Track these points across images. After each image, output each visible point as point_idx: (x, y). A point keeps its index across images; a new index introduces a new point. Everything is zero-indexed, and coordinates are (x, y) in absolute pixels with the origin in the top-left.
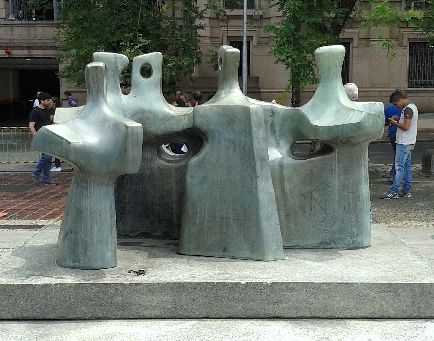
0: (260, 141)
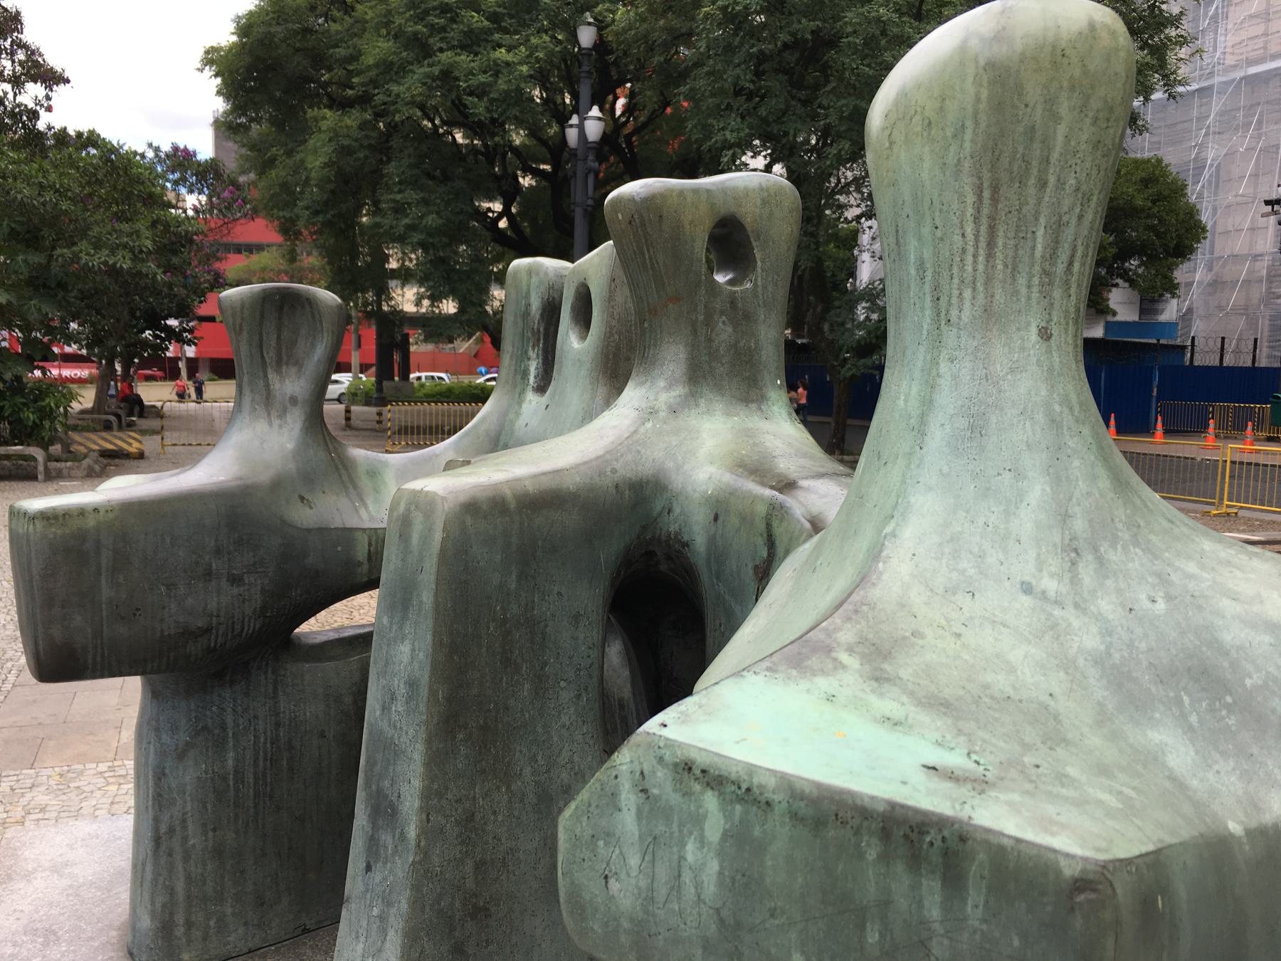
0: (393, 698)
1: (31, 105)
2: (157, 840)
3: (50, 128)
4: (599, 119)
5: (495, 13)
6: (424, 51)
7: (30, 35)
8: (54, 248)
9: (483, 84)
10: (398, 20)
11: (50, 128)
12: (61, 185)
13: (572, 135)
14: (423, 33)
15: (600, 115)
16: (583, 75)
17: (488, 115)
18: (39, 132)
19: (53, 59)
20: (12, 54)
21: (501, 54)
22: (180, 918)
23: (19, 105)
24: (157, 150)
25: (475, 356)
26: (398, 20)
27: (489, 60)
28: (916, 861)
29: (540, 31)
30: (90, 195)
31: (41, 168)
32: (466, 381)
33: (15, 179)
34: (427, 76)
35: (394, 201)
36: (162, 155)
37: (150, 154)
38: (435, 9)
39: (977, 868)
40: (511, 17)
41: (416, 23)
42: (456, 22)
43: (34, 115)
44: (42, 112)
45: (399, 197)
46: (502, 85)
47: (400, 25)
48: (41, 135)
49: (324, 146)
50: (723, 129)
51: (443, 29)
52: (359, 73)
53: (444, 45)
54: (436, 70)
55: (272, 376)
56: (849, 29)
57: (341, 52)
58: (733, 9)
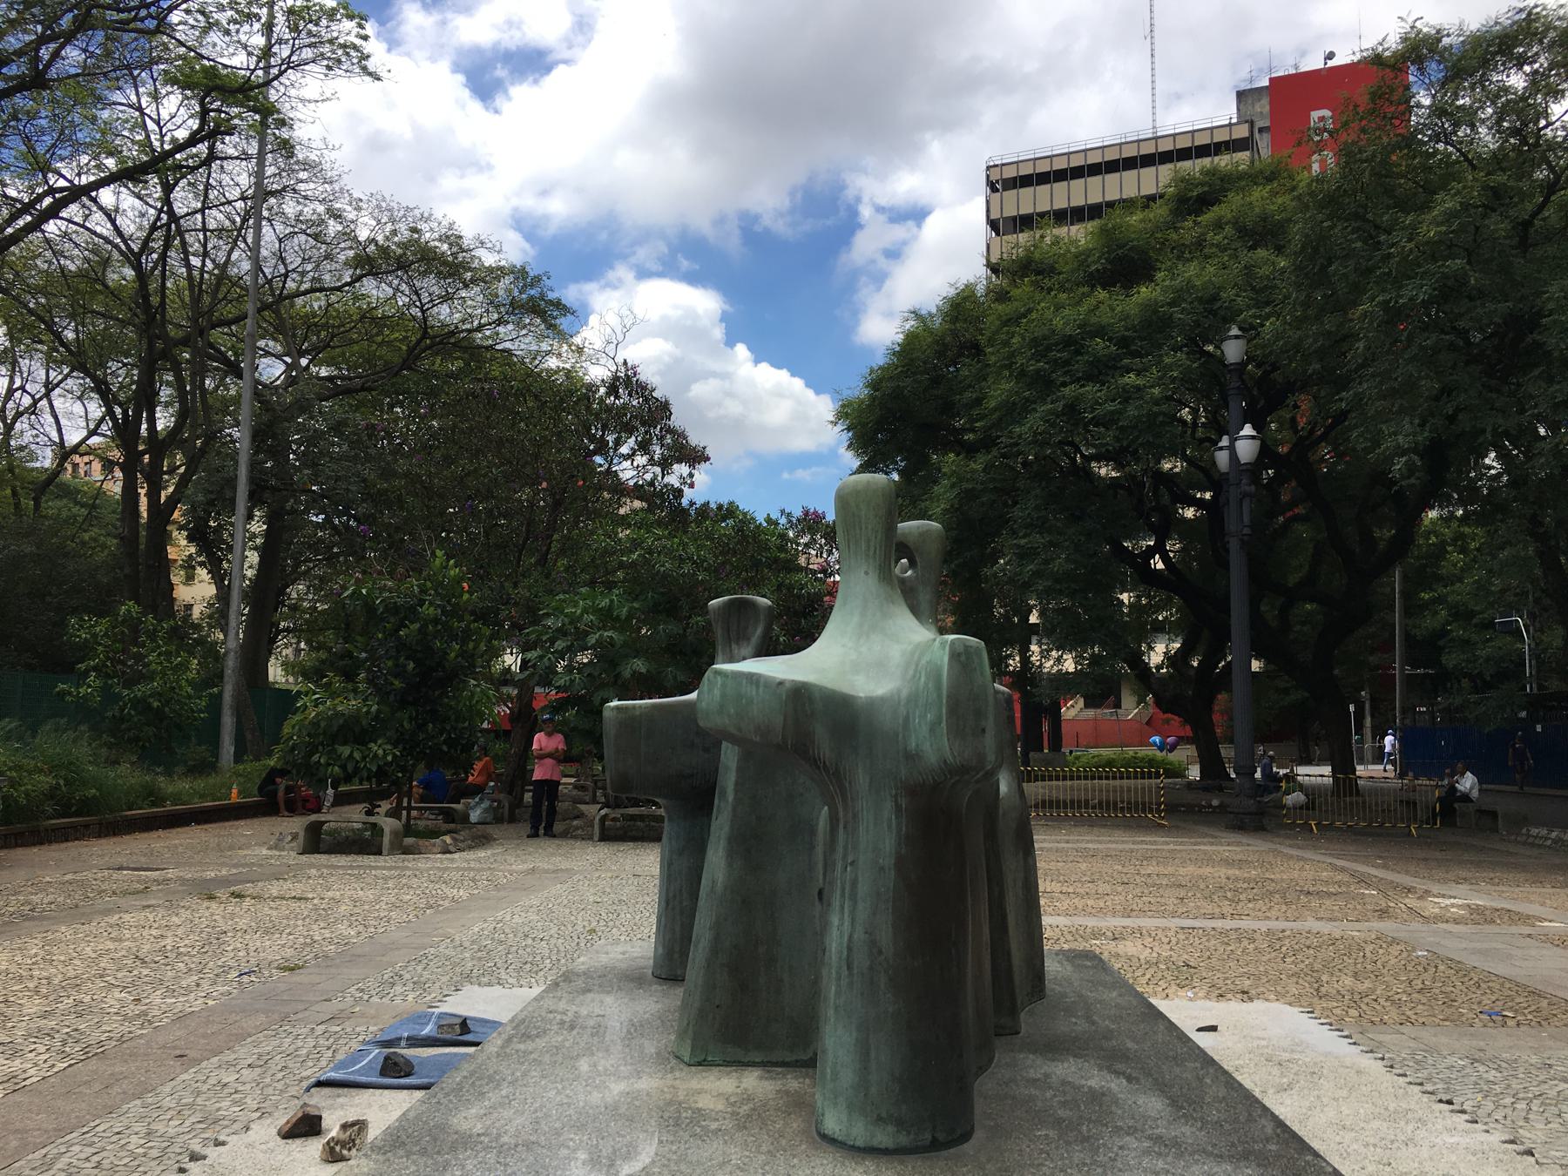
1: (677, 485)
2: (667, 903)
3: (692, 503)
4: (1253, 437)
5: (1124, 338)
6: (1044, 384)
7: (676, 421)
8: (690, 617)
9: (1112, 413)
10: (1020, 360)
11: (692, 503)
12: (698, 556)
13: (1222, 458)
14: (1045, 370)
15: (1254, 433)
16: (1231, 392)
17: (1117, 445)
18: (683, 509)
19: (694, 439)
20: (661, 438)
21: (1131, 378)
22: (677, 949)
23: (666, 486)
24: (789, 515)
25: (1148, 723)
26: (1020, 360)
27: (1117, 387)
28: (751, 683)
29: (1176, 349)
30: (723, 563)
31: (681, 543)
32: (1131, 753)
33: (659, 553)
34: (1050, 412)
35: (1018, 546)
36: (794, 520)
37: (783, 521)
38: (1057, 344)
39: (761, 684)
40: (1142, 339)
41: (1039, 361)
42: (1081, 354)
43: (679, 493)
44: (686, 489)
45: (1023, 542)
46: (1132, 411)
47: (1022, 364)
48: (685, 512)
49: (945, 492)
50: (1395, 434)
51: (1067, 363)
52: (982, 417)
53: (1067, 379)
54: (1060, 406)
55: (734, 646)
56: (1551, 306)
57: (969, 395)
58: (1397, 302)
